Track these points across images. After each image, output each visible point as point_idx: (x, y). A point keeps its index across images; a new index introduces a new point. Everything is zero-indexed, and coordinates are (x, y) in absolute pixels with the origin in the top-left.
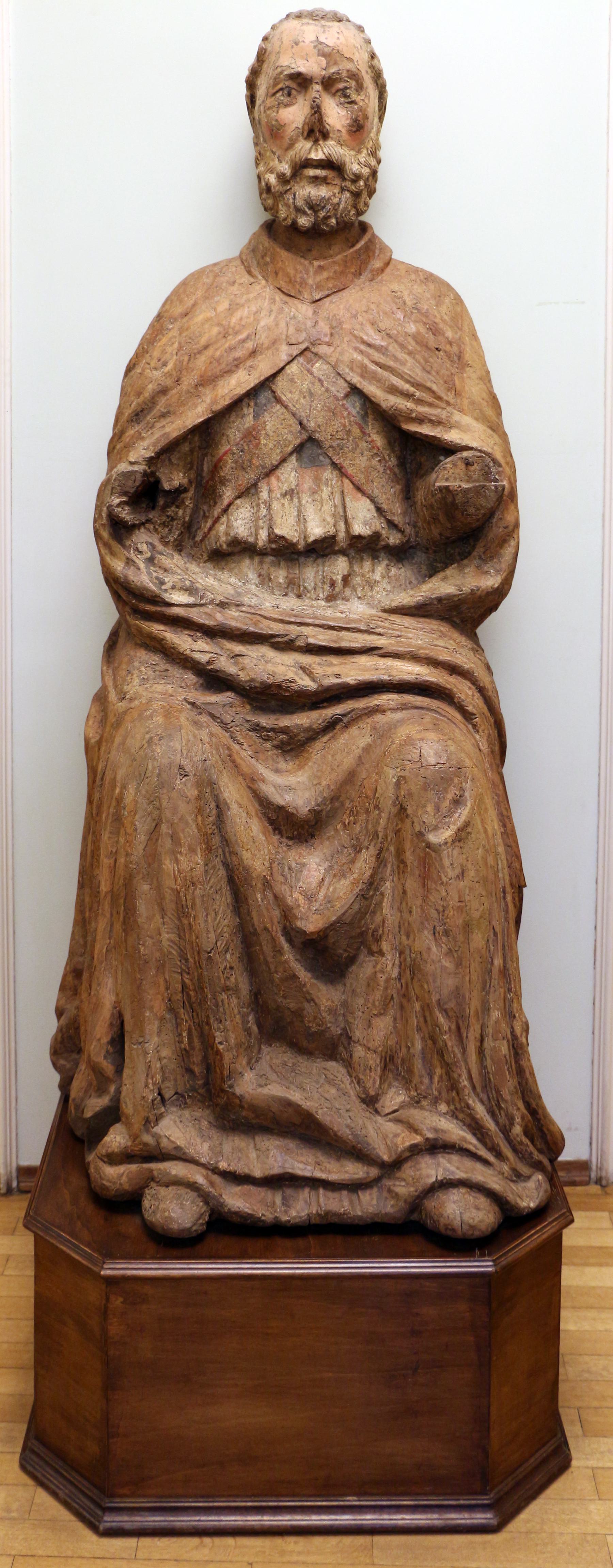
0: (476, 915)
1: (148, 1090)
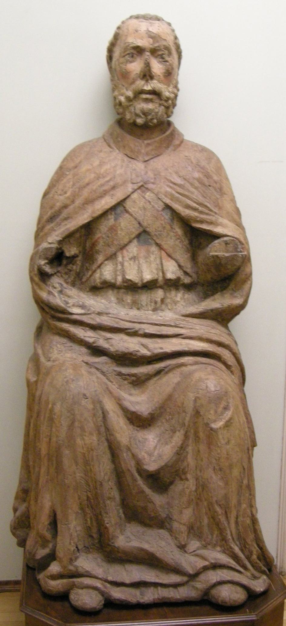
0: (235, 461)
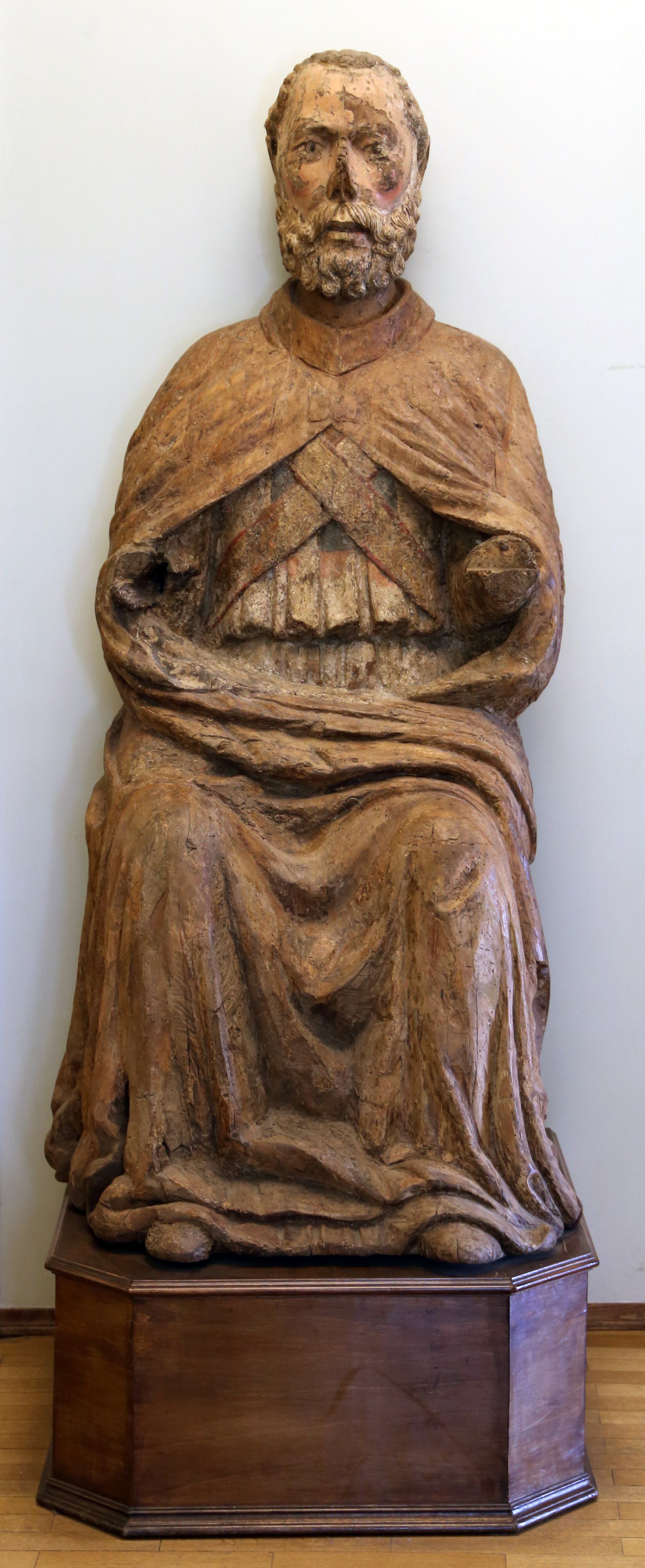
1: (152, 1138)
